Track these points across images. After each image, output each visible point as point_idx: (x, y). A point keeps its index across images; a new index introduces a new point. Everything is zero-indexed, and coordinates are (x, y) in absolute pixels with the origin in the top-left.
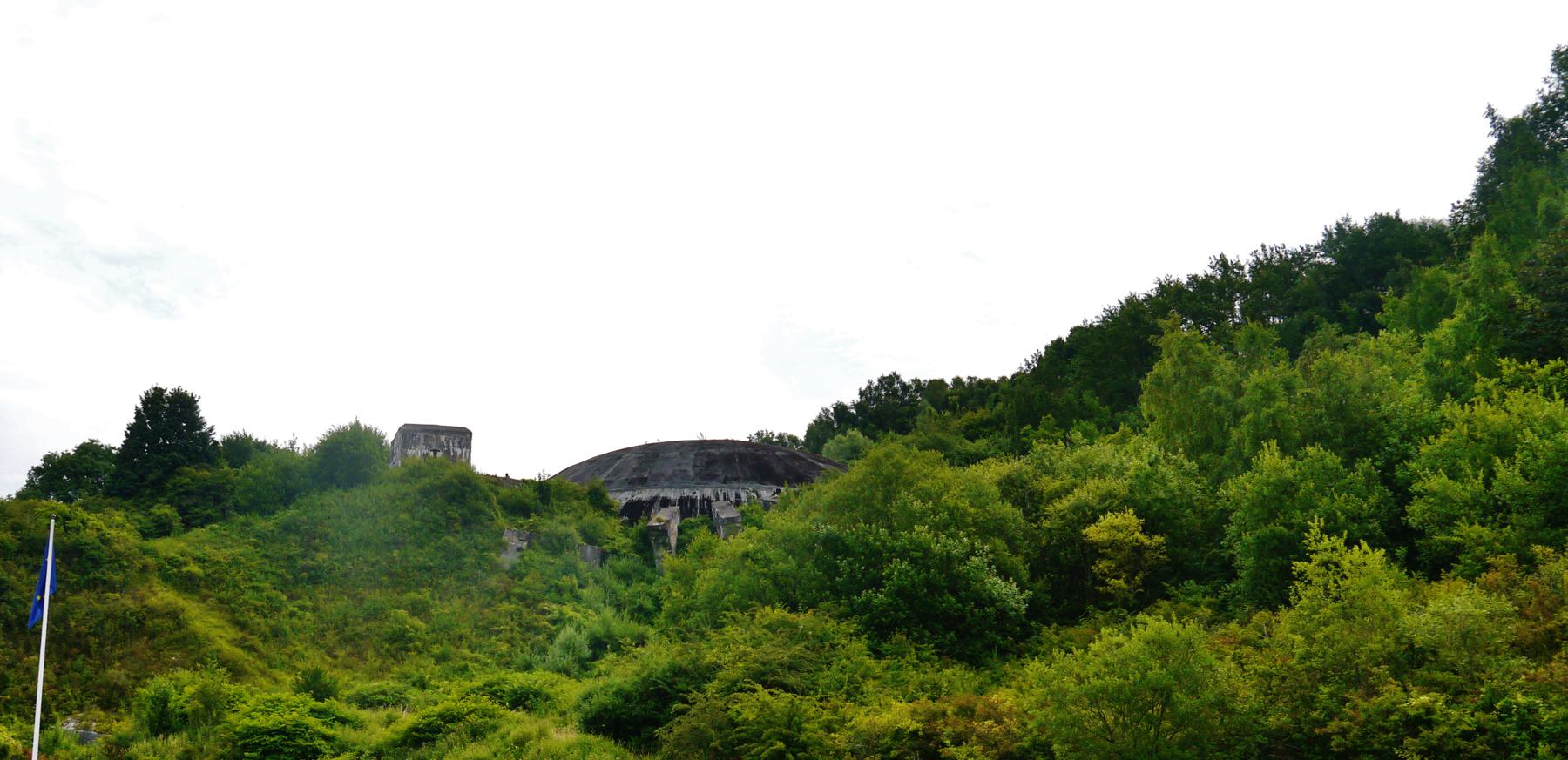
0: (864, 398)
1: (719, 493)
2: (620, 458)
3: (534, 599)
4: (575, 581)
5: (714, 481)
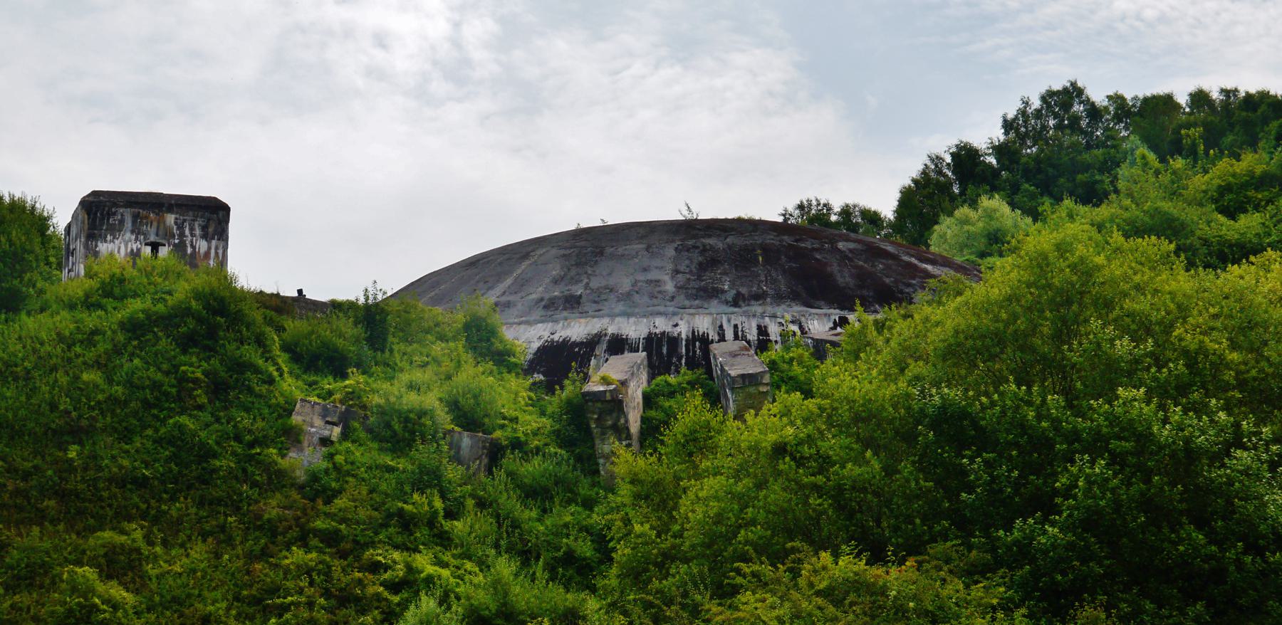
1: (725, 326)
2: (526, 256)
3: (356, 542)
5: (715, 302)
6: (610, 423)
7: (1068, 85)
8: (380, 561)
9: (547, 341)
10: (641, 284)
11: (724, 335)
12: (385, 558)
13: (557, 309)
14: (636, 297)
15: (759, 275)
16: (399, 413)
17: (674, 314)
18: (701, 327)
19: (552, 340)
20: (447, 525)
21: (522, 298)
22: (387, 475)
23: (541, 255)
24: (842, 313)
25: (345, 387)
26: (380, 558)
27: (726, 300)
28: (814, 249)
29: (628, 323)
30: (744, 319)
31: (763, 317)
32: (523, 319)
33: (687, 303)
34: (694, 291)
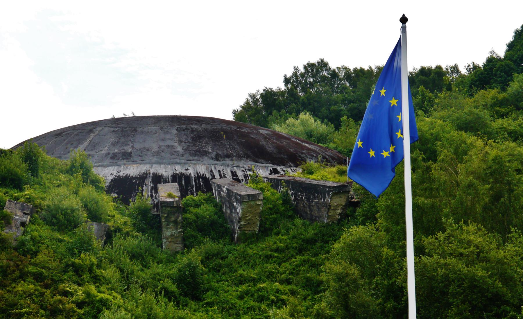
0: (290, 86)
1: (214, 171)
2: (91, 131)
3: (52, 280)
4: (94, 260)
5: (206, 158)
6: (173, 219)
7: (320, 61)
8: (68, 291)
9: (116, 176)
10: (163, 147)
11: (214, 176)
12: (70, 288)
13: (118, 159)
14: (163, 154)
15: (225, 145)
16: (62, 210)
17: (185, 164)
18: (201, 170)
19: (119, 176)
20: (98, 272)
21: (96, 153)
22: (59, 244)
23: (100, 131)
24: (274, 166)
25: (25, 195)
26: (68, 289)
27: (211, 157)
28: (249, 133)
29: (161, 168)
30: (223, 167)
31: (233, 167)
32: (99, 164)
33: (191, 158)
34: (193, 152)
